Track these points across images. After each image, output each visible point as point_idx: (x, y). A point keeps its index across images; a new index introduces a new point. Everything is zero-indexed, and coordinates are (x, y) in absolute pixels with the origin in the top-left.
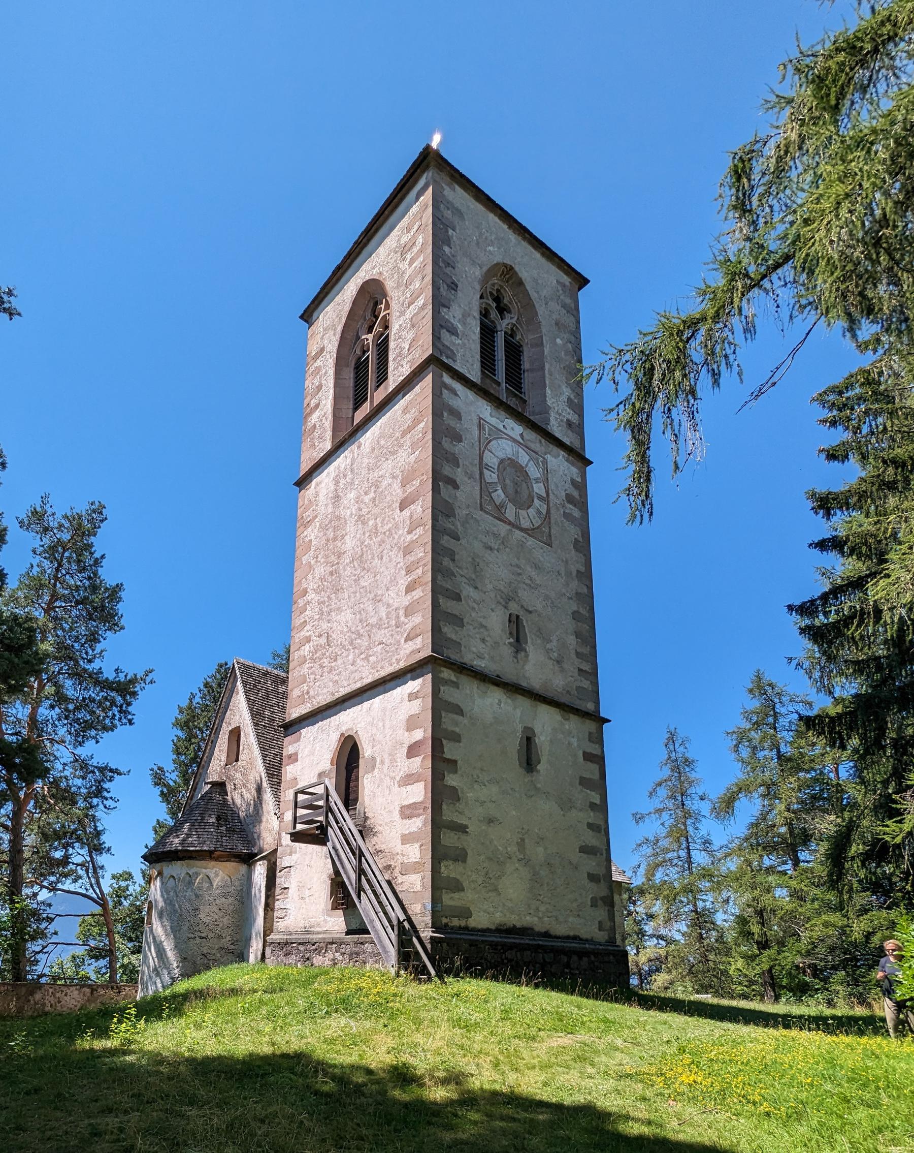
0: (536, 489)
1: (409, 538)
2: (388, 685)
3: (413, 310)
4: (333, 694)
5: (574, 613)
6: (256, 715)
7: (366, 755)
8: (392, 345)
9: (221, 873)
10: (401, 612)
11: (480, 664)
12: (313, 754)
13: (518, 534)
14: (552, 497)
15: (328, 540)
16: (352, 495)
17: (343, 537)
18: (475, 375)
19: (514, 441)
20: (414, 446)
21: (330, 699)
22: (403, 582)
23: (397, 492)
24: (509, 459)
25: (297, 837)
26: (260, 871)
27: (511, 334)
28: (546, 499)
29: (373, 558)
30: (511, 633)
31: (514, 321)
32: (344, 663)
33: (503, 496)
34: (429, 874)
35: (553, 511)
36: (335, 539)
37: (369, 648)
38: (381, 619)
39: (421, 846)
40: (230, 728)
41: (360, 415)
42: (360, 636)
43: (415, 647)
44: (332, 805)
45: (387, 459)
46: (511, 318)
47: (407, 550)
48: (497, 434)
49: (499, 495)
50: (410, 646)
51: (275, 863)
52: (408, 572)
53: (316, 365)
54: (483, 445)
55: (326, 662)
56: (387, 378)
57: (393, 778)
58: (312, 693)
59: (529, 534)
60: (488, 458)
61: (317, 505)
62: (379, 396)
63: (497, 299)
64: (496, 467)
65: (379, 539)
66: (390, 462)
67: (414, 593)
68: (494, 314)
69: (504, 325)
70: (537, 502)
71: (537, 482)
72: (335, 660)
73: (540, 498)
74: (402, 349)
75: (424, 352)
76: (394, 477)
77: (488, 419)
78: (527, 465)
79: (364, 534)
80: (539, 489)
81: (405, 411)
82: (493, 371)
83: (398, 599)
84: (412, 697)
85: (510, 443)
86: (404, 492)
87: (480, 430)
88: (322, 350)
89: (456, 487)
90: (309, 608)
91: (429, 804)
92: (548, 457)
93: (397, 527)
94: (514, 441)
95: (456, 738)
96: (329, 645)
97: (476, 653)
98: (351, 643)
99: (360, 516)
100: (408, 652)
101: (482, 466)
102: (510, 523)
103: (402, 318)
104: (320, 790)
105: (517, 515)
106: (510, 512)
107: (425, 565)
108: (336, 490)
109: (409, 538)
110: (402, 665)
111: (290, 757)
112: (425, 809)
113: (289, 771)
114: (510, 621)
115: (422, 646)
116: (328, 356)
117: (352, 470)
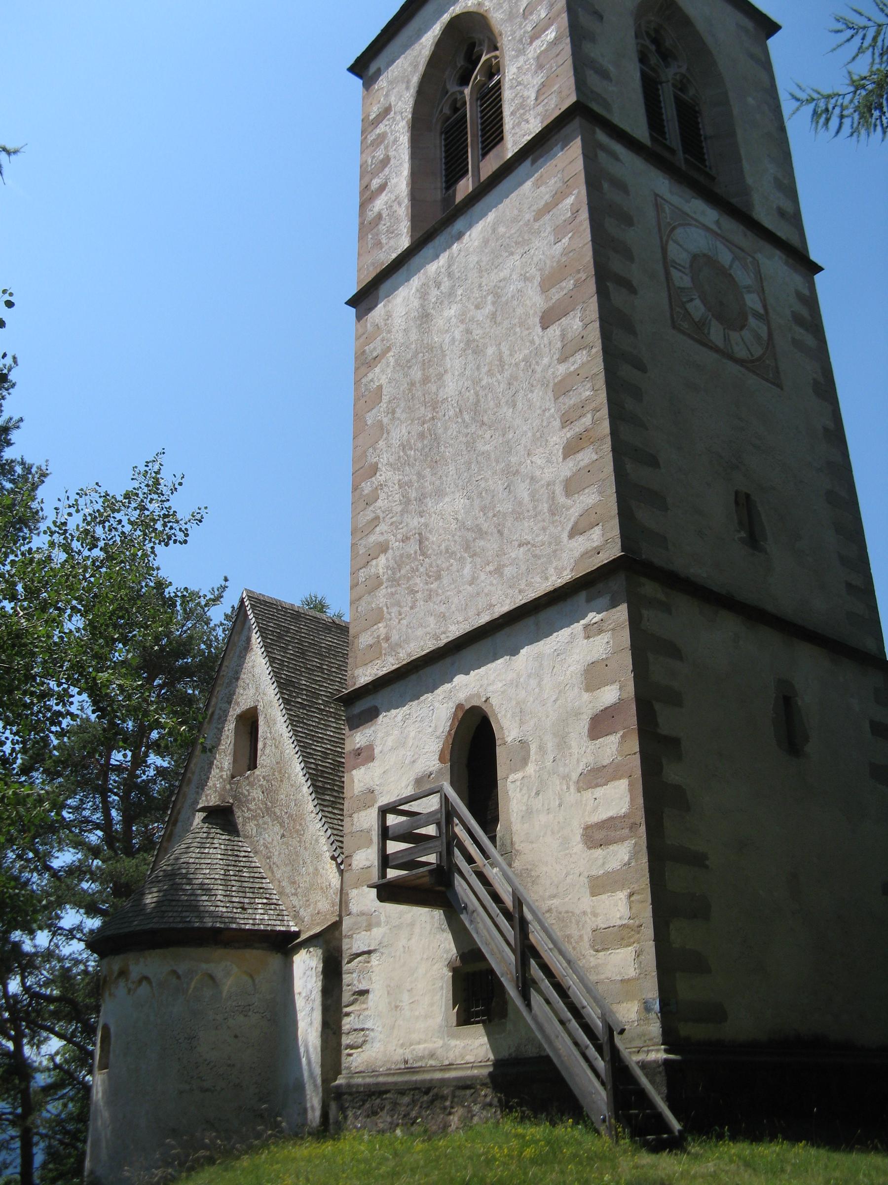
0: (749, 303)
1: (562, 369)
2: (543, 616)
3: (539, 46)
4: (437, 638)
6: (285, 686)
7: (509, 740)
8: (507, 94)
9: (235, 969)
10: (559, 489)
11: (699, 572)
12: (404, 745)
15: (412, 384)
16: (452, 312)
17: (440, 377)
20: (558, 233)
21: (430, 646)
22: (558, 438)
23: (535, 300)
24: (704, 255)
25: (389, 892)
26: (306, 968)
27: (682, 86)
28: (764, 317)
29: (498, 405)
31: (683, 70)
32: (454, 581)
33: (702, 309)
34: (650, 947)
36: (426, 380)
37: (501, 553)
38: (520, 504)
39: (631, 895)
41: (465, 187)
42: (481, 533)
43: (589, 545)
44: (459, 830)
45: (512, 254)
46: (679, 67)
47: (561, 389)
49: (697, 308)
50: (581, 544)
51: (339, 951)
52: (566, 421)
53: (378, 131)
55: (419, 582)
56: (502, 139)
57: (566, 777)
58: (395, 637)
60: (673, 251)
61: (389, 332)
62: (490, 165)
63: (657, 41)
64: (687, 266)
65: (507, 374)
66: (517, 257)
67: (579, 456)
68: (654, 59)
69: (670, 74)
70: (752, 321)
71: (749, 292)
72: (438, 577)
73: (756, 315)
74: (524, 99)
75: (562, 100)
76: (526, 279)
77: (668, 196)
78: (731, 266)
79: (478, 368)
80: (752, 301)
82: (663, 133)
83: (549, 465)
86: (548, 299)
87: (658, 211)
88: (387, 110)
89: (633, 290)
90: (382, 496)
91: (640, 817)
92: (759, 256)
93: (538, 353)
95: (674, 699)
96: (423, 554)
98: (467, 548)
99: (468, 343)
100: (577, 554)
101: (667, 264)
102: (716, 350)
103: (522, 59)
104: (431, 804)
105: (726, 339)
106: (716, 332)
107: (596, 410)
108: (422, 306)
109: (562, 369)
110: (567, 577)
111: (358, 752)
112: (633, 827)
113: (359, 779)
114: (737, 503)
115: (602, 543)
116: (398, 118)
117: (450, 275)
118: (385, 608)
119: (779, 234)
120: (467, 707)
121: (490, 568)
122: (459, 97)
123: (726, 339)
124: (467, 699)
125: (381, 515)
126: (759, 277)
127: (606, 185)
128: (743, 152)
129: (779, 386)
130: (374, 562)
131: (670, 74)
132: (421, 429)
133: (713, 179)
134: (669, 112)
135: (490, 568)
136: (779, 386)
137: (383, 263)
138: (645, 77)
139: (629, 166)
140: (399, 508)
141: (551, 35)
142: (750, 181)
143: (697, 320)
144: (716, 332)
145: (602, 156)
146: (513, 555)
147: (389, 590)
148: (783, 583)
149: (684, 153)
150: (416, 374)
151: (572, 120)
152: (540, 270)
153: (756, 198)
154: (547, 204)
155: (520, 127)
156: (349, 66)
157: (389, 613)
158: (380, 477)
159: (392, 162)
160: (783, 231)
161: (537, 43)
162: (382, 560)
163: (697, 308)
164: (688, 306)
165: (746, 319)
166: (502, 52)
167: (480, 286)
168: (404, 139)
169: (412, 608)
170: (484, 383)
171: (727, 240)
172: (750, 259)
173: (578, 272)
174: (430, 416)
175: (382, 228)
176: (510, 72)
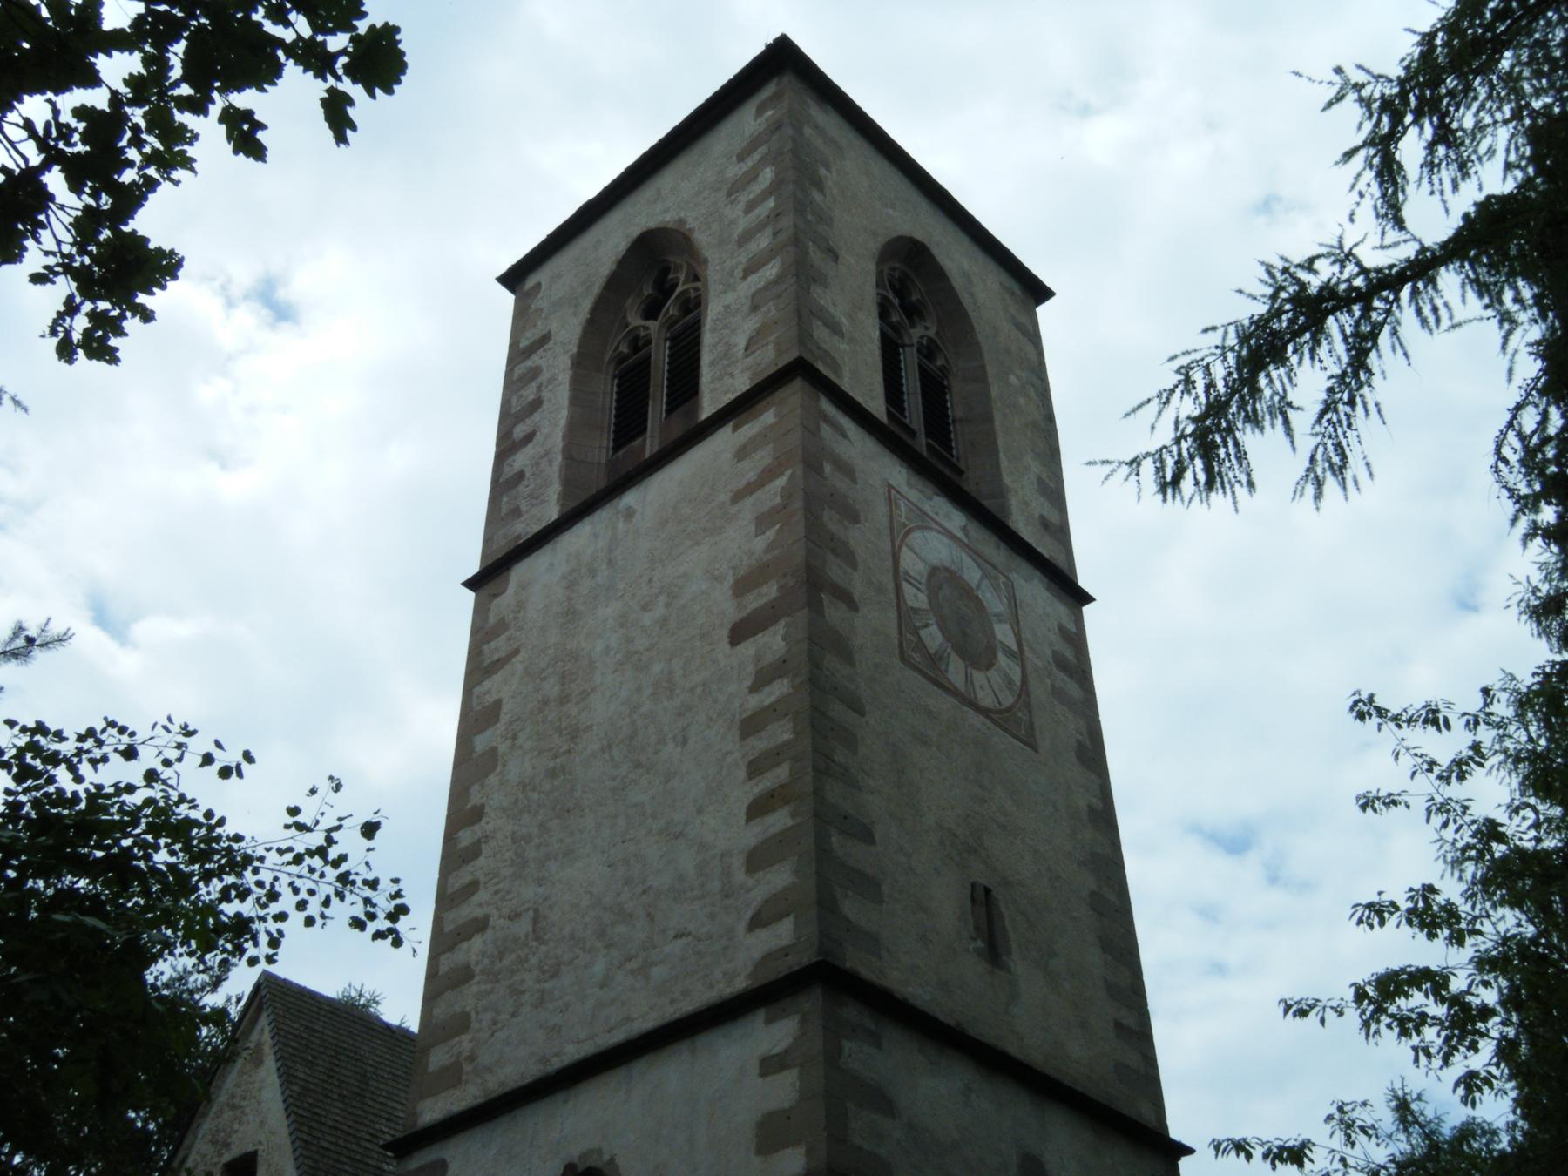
4: (544, 1060)
5: (1093, 894)
8: (708, 338)
10: (738, 863)
11: (918, 993)
13: (976, 720)
14: (1028, 654)
17: (584, 695)
18: (877, 406)
19: (952, 537)
20: (762, 522)
21: (533, 1071)
22: (744, 793)
24: (946, 569)
30: (977, 928)
31: (931, 333)
33: (939, 638)
35: (1031, 681)
36: (563, 700)
40: (227, 1157)
45: (698, 543)
47: (750, 726)
48: (924, 521)
49: (933, 637)
54: (898, 535)
59: (993, 721)
60: (908, 561)
70: (1002, 660)
71: (1000, 621)
72: (555, 974)
73: (1008, 652)
77: (904, 489)
78: (978, 586)
79: (639, 689)
80: (1004, 633)
81: (742, 453)
82: (902, 410)
84: (770, 1065)
85: (945, 540)
88: (545, 339)
89: (852, 605)
92: (1014, 576)
94: (952, 537)
96: (537, 939)
97: (907, 972)
100: (757, 954)
102: (952, 691)
105: (969, 680)
106: (956, 670)
110: (740, 984)
114: (973, 900)
118: (473, 1014)
119: (1040, 550)
120: (581, 1168)
121: (633, 965)
122: (642, 333)
123: (969, 680)
124: (582, 1157)
125: (482, 879)
126: (1014, 604)
127: (828, 468)
128: (1000, 442)
129: (1033, 747)
130: (465, 945)
131: (917, 333)
132: (552, 764)
133: (960, 472)
134: (911, 383)
135: (633, 965)
136: (1033, 747)
137: (519, 537)
138: (884, 336)
139: (858, 447)
140: (507, 872)
141: (771, 271)
142: (1007, 480)
143: (932, 652)
144: (956, 670)
145: (826, 430)
146: (667, 949)
147: (483, 987)
148: (1034, 1021)
149: (927, 436)
150: (551, 688)
151: (792, 379)
152: (734, 568)
153: (1014, 502)
154: (749, 484)
155: (719, 384)
156: (499, 274)
157: (480, 1021)
158: (486, 825)
159: (545, 406)
160: (1045, 548)
161: (753, 278)
162: (477, 943)
163: (933, 637)
164: (922, 633)
165: (995, 657)
166: (706, 286)
167: (650, 580)
168: (565, 377)
169: (513, 1015)
170: (644, 710)
171: (976, 553)
172: (1003, 579)
173: (785, 575)
174: (566, 748)
175: (523, 489)
176: (713, 310)
